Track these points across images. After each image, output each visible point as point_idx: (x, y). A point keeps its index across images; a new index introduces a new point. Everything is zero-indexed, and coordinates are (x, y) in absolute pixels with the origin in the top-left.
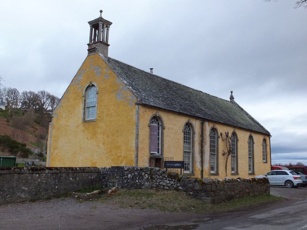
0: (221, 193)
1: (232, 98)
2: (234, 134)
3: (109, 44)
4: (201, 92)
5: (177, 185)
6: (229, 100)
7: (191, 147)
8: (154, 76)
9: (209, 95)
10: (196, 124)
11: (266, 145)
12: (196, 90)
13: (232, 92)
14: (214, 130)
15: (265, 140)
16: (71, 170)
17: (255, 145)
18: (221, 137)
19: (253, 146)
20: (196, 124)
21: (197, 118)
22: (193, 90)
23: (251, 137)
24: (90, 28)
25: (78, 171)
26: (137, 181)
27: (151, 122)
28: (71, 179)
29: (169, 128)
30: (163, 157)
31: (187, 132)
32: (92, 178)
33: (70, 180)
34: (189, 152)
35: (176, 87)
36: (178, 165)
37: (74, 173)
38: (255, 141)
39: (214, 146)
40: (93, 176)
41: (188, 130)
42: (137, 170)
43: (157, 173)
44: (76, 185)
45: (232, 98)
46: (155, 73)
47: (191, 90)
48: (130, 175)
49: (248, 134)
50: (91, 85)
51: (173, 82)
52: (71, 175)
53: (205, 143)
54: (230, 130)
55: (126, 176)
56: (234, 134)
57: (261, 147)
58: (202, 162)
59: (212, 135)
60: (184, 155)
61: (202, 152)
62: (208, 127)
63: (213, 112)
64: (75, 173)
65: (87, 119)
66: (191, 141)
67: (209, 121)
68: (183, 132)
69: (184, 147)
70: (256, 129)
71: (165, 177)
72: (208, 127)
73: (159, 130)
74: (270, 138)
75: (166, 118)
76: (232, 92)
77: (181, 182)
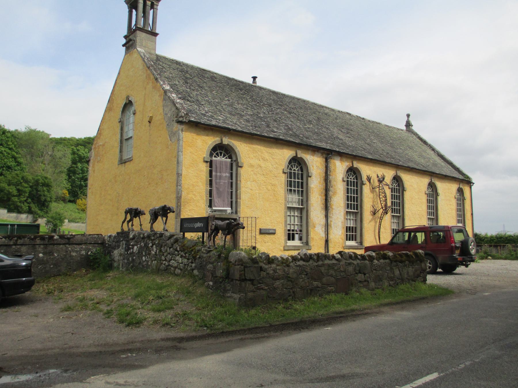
0: (278, 283)
1: (408, 125)
2: (397, 179)
3: (157, 32)
4: (348, 113)
5: (191, 266)
6: (404, 128)
7: (305, 200)
8: (261, 88)
9: (363, 119)
10: (315, 163)
11: (464, 199)
12: (339, 111)
13: (408, 116)
14: (353, 171)
15: (460, 191)
16: (40, 239)
17: (439, 198)
18: (368, 183)
19: (436, 199)
20: (315, 163)
21: (315, 149)
22: (333, 110)
23: (432, 186)
24: (127, 10)
25: (56, 242)
26: (144, 258)
27: (288, 166)
28: (41, 255)
29: (252, 166)
30: (238, 216)
31: (351, 181)
32: (89, 253)
33: (39, 256)
34: (398, 216)
35: (294, 104)
36: (199, 225)
37: (46, 245)
38: (440, 191)
39: (355, 199)
40: (94, 250)
41: (354, 179)
42: (143, 238)
43: (167, 242)
44: (52, 266)
45: (408, 125)
46: (259, 83)
47: (327, 111)
48: (135, 247)
49: (425, 181)
50: (128, 102)
51: (293, 98)
52: (40, 249)
53: (335, 193)
54: (389, 174)
55: (132, 250)
56: (397, 179)
57: (454, 202)
58: (327, 226)
59: (351, 179)
60: (286, 213)
61: (327, 207)
62: (340, 167)
63: (361, 143)
64: (50, 244)
65: (125, 157)
66: (304, 189)
67: (341, 155)
68: (426, 194)
69: (287, 201)
70: (448, 171)
71: (176, 250)
72: (340, 167)
73: (232, 169)
74: (471, 188)
75: (243, 149)
76: (408, 116)
77: (197, 261)
